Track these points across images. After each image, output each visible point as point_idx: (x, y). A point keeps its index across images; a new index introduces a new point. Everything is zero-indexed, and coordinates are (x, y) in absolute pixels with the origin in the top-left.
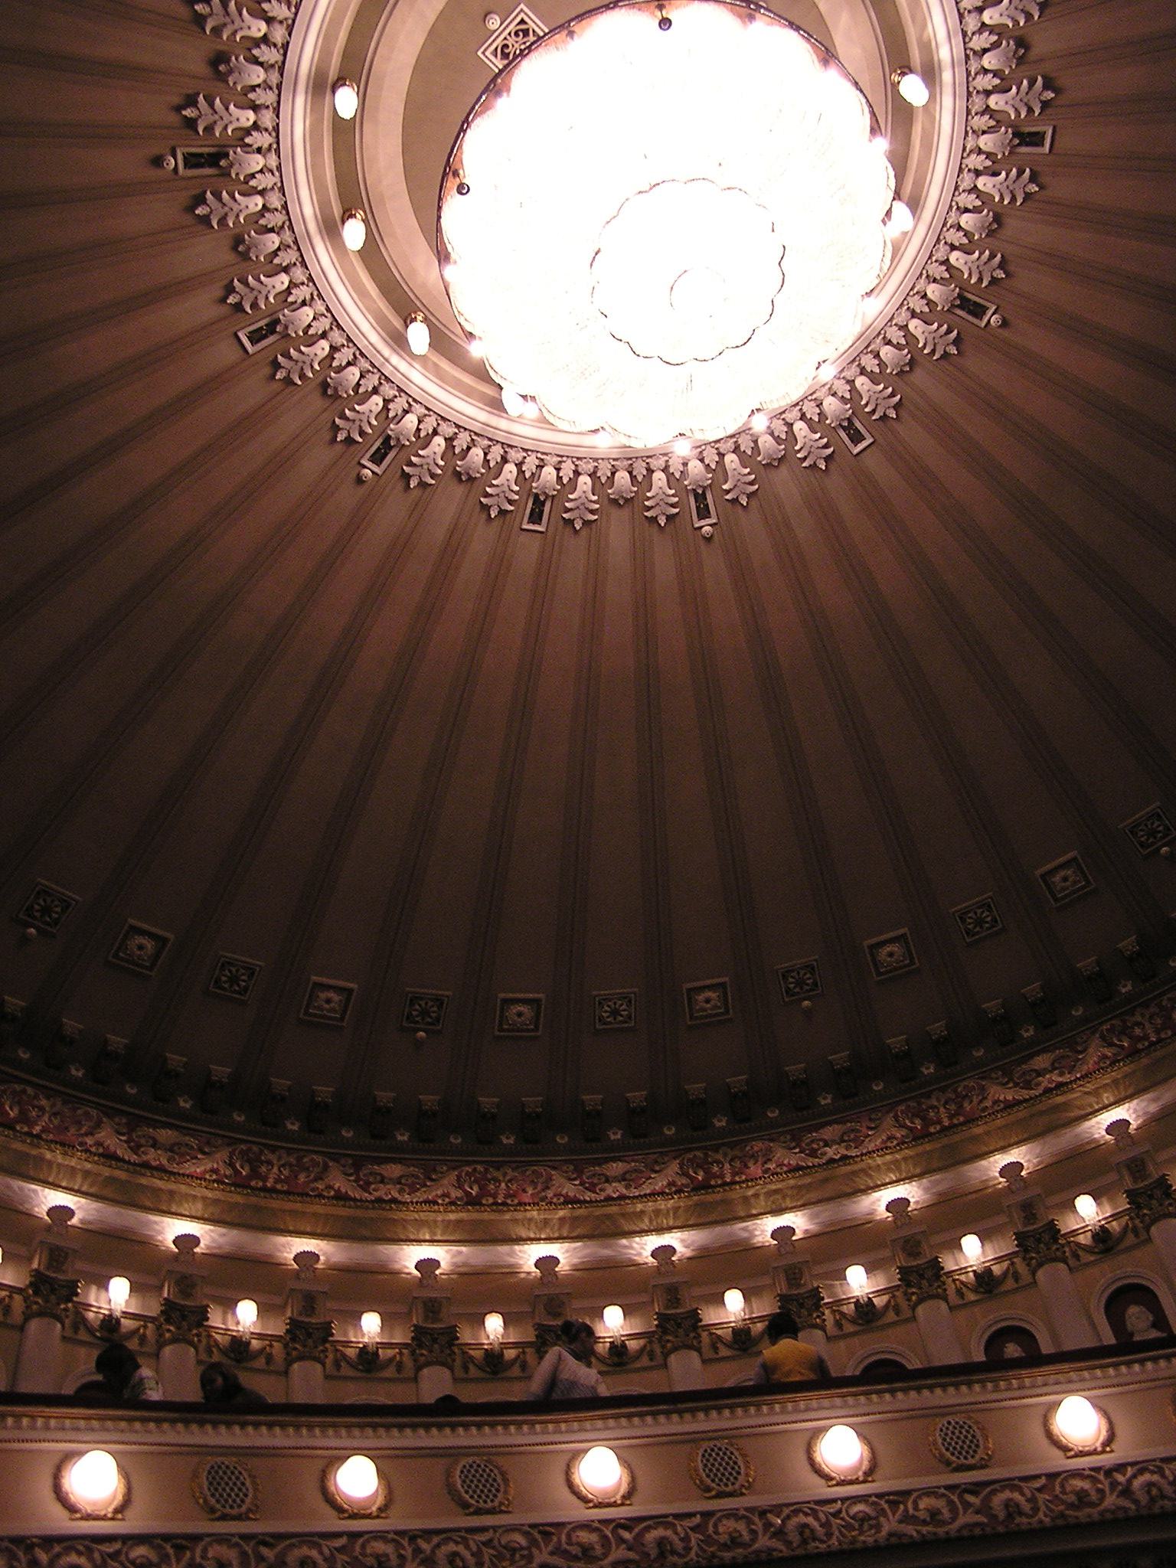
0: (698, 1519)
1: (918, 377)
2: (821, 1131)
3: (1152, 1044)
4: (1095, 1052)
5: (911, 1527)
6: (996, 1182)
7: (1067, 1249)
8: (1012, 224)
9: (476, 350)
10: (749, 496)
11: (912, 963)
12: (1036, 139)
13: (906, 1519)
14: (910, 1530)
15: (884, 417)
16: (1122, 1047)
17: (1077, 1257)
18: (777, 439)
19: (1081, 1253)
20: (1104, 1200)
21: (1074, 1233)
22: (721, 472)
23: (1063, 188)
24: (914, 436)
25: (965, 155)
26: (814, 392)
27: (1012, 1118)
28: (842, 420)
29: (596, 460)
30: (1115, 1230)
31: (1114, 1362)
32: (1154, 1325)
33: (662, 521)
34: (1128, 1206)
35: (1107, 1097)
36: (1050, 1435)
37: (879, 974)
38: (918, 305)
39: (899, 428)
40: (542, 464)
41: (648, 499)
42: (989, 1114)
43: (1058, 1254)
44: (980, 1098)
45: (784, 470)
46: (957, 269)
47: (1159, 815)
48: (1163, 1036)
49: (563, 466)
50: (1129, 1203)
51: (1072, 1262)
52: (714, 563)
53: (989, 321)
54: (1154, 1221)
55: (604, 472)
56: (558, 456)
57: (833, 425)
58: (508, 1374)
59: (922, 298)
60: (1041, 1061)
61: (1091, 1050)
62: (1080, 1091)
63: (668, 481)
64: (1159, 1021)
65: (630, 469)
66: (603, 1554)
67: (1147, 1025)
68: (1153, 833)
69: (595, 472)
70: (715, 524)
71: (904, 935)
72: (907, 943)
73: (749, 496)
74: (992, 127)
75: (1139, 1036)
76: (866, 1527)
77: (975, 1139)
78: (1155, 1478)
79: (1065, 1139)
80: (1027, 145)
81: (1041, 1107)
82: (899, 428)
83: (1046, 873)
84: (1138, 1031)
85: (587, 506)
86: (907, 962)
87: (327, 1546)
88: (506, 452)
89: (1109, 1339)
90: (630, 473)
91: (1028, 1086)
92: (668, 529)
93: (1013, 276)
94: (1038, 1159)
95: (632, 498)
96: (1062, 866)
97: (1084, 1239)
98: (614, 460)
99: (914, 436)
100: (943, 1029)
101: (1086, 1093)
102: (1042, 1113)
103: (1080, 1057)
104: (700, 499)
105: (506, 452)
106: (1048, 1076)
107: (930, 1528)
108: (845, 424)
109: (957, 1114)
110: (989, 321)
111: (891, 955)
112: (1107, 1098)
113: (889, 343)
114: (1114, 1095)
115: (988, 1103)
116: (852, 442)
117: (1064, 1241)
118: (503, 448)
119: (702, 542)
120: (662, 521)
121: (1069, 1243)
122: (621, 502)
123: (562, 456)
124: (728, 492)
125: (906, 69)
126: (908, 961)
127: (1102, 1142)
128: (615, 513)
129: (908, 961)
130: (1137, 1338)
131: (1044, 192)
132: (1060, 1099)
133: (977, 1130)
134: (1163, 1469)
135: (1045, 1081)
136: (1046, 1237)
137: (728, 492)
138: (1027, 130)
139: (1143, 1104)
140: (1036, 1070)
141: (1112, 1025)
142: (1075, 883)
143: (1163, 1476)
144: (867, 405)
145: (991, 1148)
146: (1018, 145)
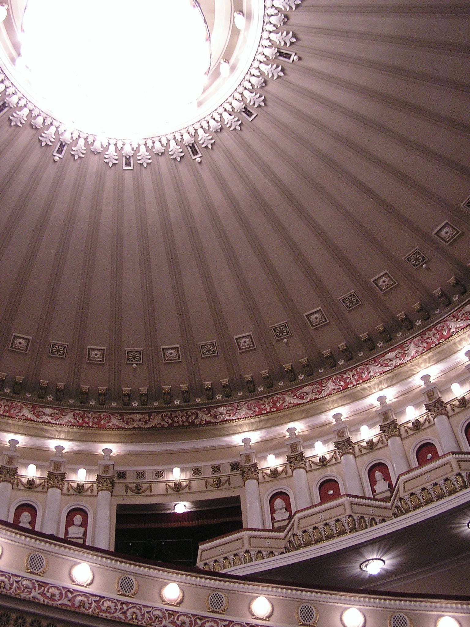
0: (98, 598)
1: (162, 159)
2: (44, 409)
3: (89, 427)
4: (69, 418)
5: (42, 597)
6: (5, 443)
7: (16, 480)
8: (224, 133)
9: (20, 37)
10: (147, 164)
11: (26, 350)
12: (249, 114)
13: (43, 594)
14: (41, 598)
15: (141, 164)
16: (78, 422)
17: (18, 485)
18: (102, 146)
19: (20, 484)
20: (39, 470)
21: (22, 476)
22: (75, 143)
23: (247, 135)
24: (147, 177)
25: (226, 102)
26: (125, 139)
27: (25, 424)
28: (128, 155)
29: (35, 106)
30: (37, 482)
31: (31, 536)
32: (30, 523)
33: (43, 144)
34: (47, 477)
35: (62, 436)
36: (70, 574)
37: (12, 347)
38: (178, 137)
39: (144, 171)
40: (15, 93)
41: (44, 133)
42: (18, 418)
43: (12, 481)
44: (19, 411)
45: (97, 157)
46: (198, 135)
47: (140, 353)
48: (94, 426)
49: (22, 100)
50: (47, 476)
51: (15, 486)
52: (51, 170)
53: (196, 159)
54: (52, 487)
55: (35, 113)
56: (23, 95)
57: (123, 155)
58: (86, 493)
59: (181, 135)
60: (48, 411)
61: (67, 417)
62: (55, 429)
63: (55, 132)
64: (96, 420)
65: (45, 119)
66: (114, 612)
67: (91, 419)
68: (134, 357)
69: (32, 110)
70: (61, 158)
71: (29, 339)
72: (28, 343)
73: (79, 157)
74: (240, 100)
75: (86, 421)
76: (26, 590)
77: (7, 423)
78: (6, 580)
79: (39, 442)
80: (246, 113)
81: (37, 426)
82: (144, 171)
83: (16, 336)
84: (87, 419)
85: (21, 120)
86: (24, 349)
87: (144, 610)
88: (5, 79)
89: (11, 520)
90: (44, 120)
91: (38, 416)
92: (44, 148)
93: (213, 150)
94: (25, 444)
95: (39, 129)
96: (98, 350)
97: (24, 480)
98: (42, 111)
99: (147, 177)
100: (22, 380)
101: (57, 431)
102: (36, 428)
103: (62, 417)
104: (62, 146)
105: (5, 79)
106: (47, 417)
107: (48, 601)
108: (128, 157)
109: (7, 412)
110: (196, 159)
111: (20, 343)
112: (62, 436)
113: (160, 142)
114: (65, 436)
115: (21, 414)
116: (126, 164)
117: (17, 477)
118: (5, 77)
119: (52, 160)
120: (43, 144)
121: (18, 479)
122: (34, 127)
123: (24, 96)
124: (73, 151)
125: (227, 61)
126: (25, 349)
127: (51, 450)
128: (29, 129)
129: (25, 349)
130: (20, 524)
131: (240, 132)
132: (46, 427)
133: (10, 421)
134: (11, 577)
135: (45, 418)
136: (11, 472)
137: (73, 151)
138: (249, 109)
139: (73, 445)
140: (44, 413)
141: (80, 413)
142: (99, 358)
143: (9, 580)
144: (139, 156)
145: (11, 431)
146: (244, 112)
